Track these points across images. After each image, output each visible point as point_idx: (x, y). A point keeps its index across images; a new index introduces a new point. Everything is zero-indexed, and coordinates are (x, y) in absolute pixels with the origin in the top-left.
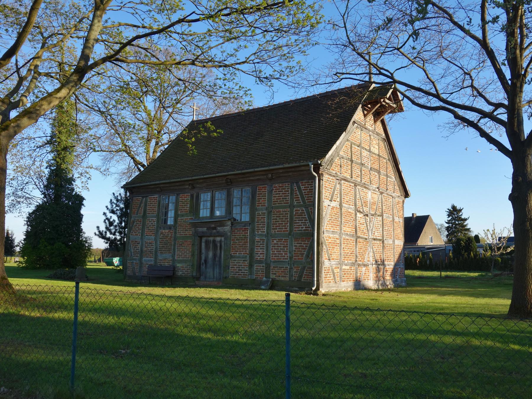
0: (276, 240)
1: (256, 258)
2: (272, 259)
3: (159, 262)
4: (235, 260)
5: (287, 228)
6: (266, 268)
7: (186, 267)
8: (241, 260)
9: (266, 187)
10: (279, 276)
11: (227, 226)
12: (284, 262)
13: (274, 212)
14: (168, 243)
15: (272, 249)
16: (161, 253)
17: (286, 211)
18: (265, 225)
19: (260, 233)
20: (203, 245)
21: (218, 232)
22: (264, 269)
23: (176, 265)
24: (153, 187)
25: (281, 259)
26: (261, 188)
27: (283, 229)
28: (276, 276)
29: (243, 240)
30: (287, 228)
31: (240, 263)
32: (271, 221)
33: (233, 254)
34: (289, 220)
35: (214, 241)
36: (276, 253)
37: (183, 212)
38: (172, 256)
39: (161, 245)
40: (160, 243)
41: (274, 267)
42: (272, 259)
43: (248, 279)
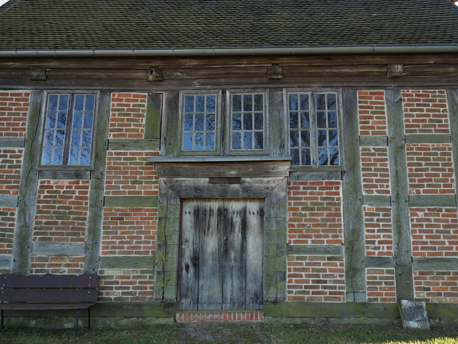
0: (424, 210)
1: (369, 253)
2: (415, 254)
3: (34, 266)
4: (304, 258)
5: (450, 186)
6: (399, 276)
7: (139, 277)
8: (323, 259)
9: (382, 93)
10: (440, 294)
11: (277, 174)
12: (449, 260)
13: (412, 149)
14: (71, 213)
15: (414, 231)
16: (41, 239)
17: (444, 149)
18: (388, 176)
19: (375, 193)
20: (188, 220)
21: (246, 190)
22: (392, 278)
23: (102, 272)
24: (18, 64)
25: (441, 254)
26: (366, 93)
27: (440, 186)
28: (428, 295)
29: (325, 209)
30: (450, 186)
31: (319, 264)
32: (404, 169)
33: (295, 242)
34: (453, 167)
35: (223, 212)
36: (424, 239)
37: (124, 135)
38: (86, 248)
39: (42, 217)
40: (39, 212)
41: (421, 273)
42: (415, 254)
43: (347, 303)
